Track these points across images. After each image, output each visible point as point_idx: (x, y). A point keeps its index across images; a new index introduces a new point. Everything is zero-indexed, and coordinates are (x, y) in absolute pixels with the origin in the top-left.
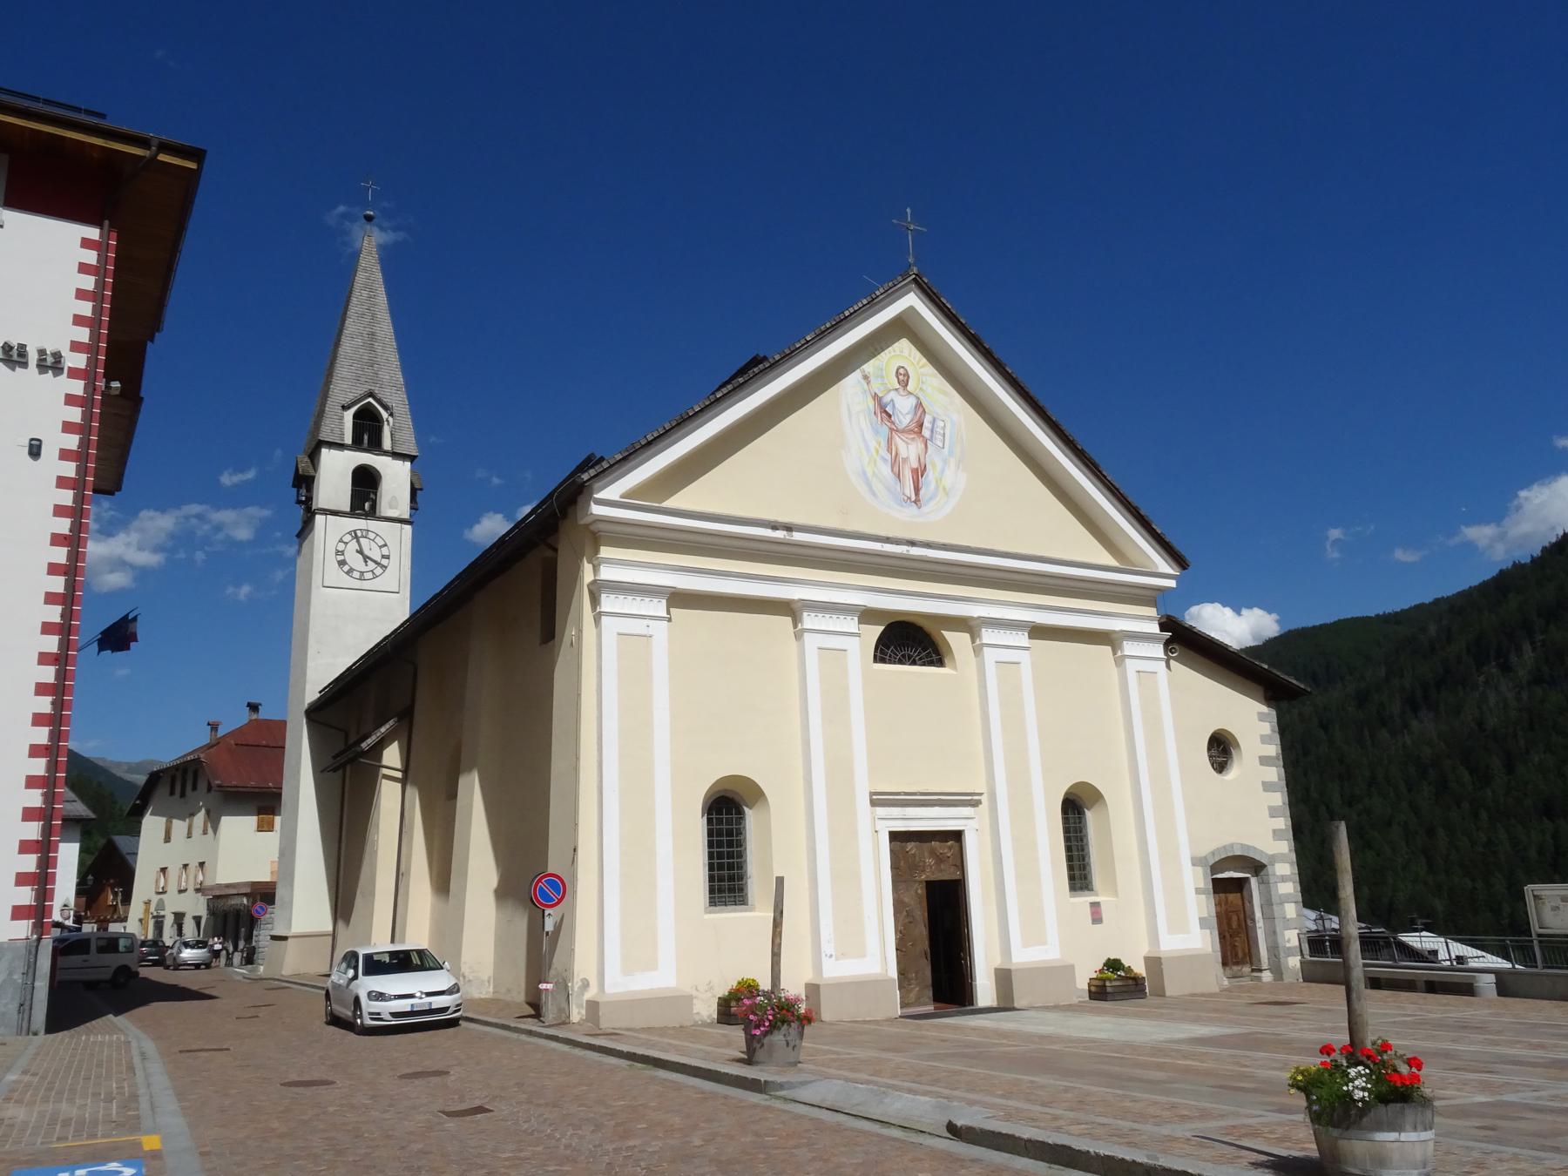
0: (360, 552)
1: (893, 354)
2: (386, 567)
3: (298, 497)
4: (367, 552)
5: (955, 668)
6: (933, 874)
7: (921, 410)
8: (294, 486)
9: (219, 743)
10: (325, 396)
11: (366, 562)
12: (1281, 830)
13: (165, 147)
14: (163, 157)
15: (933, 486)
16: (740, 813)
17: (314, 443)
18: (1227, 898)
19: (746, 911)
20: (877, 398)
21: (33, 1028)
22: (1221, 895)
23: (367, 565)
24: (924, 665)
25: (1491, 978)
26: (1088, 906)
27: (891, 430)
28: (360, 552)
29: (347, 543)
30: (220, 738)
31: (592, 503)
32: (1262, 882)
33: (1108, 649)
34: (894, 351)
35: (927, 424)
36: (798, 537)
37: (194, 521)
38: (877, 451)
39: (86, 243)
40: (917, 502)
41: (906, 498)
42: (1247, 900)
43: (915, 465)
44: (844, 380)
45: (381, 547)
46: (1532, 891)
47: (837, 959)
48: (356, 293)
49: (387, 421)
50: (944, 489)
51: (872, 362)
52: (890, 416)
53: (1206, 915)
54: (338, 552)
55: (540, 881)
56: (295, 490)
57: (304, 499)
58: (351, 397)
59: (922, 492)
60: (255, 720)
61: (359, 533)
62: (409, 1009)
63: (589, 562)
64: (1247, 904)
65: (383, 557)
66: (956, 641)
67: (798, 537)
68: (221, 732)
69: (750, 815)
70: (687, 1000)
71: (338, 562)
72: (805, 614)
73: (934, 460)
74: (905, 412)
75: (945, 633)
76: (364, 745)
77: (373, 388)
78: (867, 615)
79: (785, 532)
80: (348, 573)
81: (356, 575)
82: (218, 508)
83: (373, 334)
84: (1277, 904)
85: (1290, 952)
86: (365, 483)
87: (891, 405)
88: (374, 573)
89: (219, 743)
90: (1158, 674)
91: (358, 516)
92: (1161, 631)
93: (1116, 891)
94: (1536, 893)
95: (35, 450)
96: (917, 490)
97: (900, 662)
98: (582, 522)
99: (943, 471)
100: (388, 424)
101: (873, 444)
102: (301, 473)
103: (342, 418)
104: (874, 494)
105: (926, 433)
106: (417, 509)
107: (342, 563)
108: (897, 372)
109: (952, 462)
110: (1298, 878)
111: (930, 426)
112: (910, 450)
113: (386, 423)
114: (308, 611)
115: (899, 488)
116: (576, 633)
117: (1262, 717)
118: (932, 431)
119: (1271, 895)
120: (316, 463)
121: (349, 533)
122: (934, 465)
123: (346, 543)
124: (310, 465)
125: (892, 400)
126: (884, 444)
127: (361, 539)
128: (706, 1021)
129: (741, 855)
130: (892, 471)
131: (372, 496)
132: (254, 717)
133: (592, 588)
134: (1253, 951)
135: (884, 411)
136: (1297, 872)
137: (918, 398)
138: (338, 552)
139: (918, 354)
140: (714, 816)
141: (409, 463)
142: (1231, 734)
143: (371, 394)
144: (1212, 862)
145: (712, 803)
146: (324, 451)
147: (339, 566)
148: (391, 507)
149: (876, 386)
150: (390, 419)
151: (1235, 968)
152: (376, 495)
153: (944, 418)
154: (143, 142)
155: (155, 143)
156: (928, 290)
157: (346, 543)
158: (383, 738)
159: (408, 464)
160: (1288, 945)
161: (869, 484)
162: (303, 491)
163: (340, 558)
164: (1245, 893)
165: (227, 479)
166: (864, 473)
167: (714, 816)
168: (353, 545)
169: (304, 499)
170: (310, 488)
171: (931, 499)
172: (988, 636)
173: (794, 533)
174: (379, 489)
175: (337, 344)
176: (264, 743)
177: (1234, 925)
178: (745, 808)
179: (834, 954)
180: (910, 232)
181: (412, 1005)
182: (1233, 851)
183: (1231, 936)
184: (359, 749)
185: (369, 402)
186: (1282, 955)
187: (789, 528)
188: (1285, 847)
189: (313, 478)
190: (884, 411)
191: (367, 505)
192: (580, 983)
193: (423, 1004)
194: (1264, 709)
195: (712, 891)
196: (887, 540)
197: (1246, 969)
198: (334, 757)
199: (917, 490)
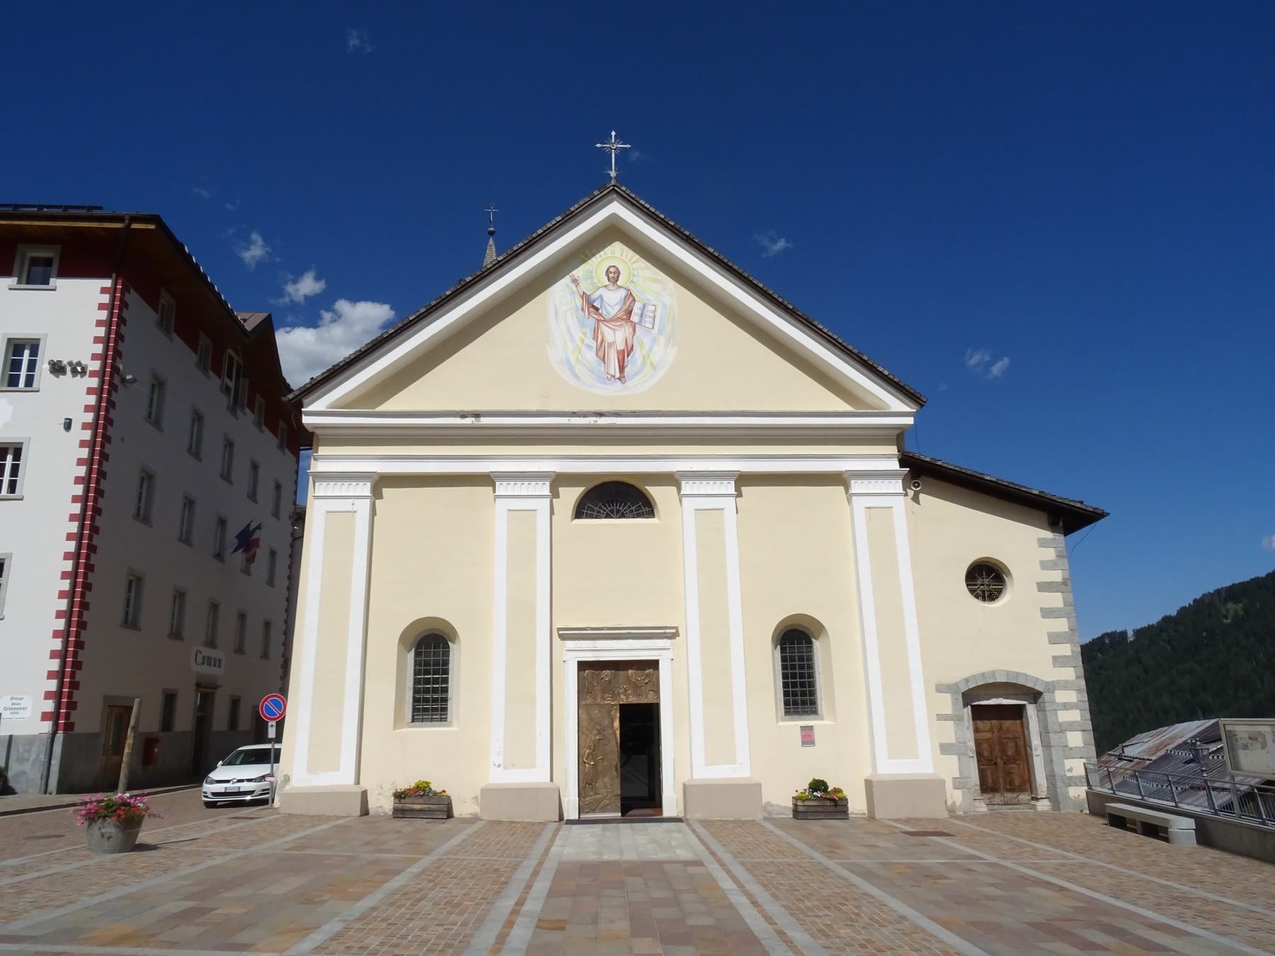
1: (604, 256)
5: (659, 519)
6: (627, 698)
7: (631, 299)
12: (1069, 656)
13: (134, 219)
14: (135, 226)
15: (639, 363)
16: (811, 643)
18: (1001, 726)
19: (445, 726)
20: (585, 297)
21: (49, 789)
22: (993, 722)
24: (634, 517)
25: (1190, 823)
26: (799, 729)
27: (598, 321)
32: (1041, 710)
33: (842, 488)
34: (605, 254)
35: (636, 310)
36: (485, 421)
38: (583, 341)
39: (104, 290)
41: (609, 377)
42: (1024, 727)
43: (621, 346)
44: (552, 287)
46: (1224, 725)
47: (505, 768)
50: (652, 364)
51: (581, 267)
52: (597, 309)
53: (953, 741)
55: (266, 700)
59: (627, 370)
62: (223, 791)
64: (1026, 732)
66: (657, 493)
67: (485, 421)
69: (817, 644)
70: (751, 790)
72: (852, 482)
74: (613, 303)
75: (647, 488)
78: (559, 481)
79: (473, 419)
84: (1056, 732)
85: (1071, 782)
87: (599, 300)
90: (725, 511)
92: (901, 467)
93: (835, 717)
94: (1228, 728)
95: (68, 425)
97: (608, 516)
99: (651, 349)
101: (578, 335)
104: (576, 376)
105: (635, 318)
108: (608, 269)
109: (662, 339)
110: (1088, 706)
111: (639, 312)
112: (616, 336)
115: (602, 369)
117: (1043, 543)
118: (642, 316)
119: (1047, 722)
122: (642, 344)
125: (601, 296)
126: (590, 333)
128: (387, 813)
129: (811, 676)
130: (597, 355)
134: (1032, 778)
135: (591, 306)
136: (1086, 699)
139: (631, 253)
140: (423, 650)
142: (1003, 564)
144: (964, 689)
145: (422, 639)
149: (585, 287)
151: (1009, 795)
153: (656, 303)
154: (119, 219)
155: (127, 217)
156: (627, 197)
160: (1069, 774)
161: (571, 368)
164: (1024, 720)
166: (568, 361)
167: (423, 650)
171: (635, 375)
172: (687, 487)
173: (482, 419)
177: (1010, 752)
178: (813, 639)
179: (502, 764)
180: (613, 151)
181: (226, 788)
182: (995, 678)
183: (1005, 763)
186: (1059, 784)
187: (477, 415)
188: (1072, 673)
190: (591, 306)
192: (282, 778)
193: (234, 787)
194: (1048, 534)
195: (786, 703)
196: (574, 414)
197: (1024, 797)
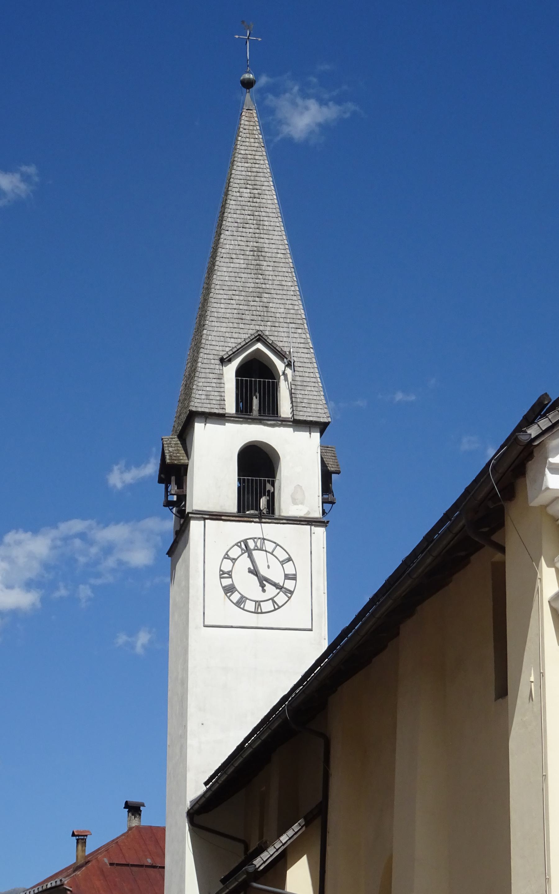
0: (254, 572)
2: (292, 592)
3: (167, 496)
4: (263, 571)
8: (160, 481)
9: (87, 863)
10: (197, 347)
11: (263, 586)
17: (184, 417)
23: (264, 591)
28: (254, 572)
29: (236, 560)
30: (90, 855)
31: (547, 471)
37: (78, 542)
45: (282, 563)
48: (234, 193)
49: (284, 373)
54: (223, 574)
56: (163, 486)
57: (175, 498)
58: (232, 344)
60: (137, 827)
61: (251, 544)
63: (549, 566)
65: (287, 577)
68: (91, 846)
71: (224, 588)
76: (258, 862)
77: (262, 328)
80: (238, 604)
81: (250, 606)
82: (105, 523)
83: (259, 250)
88: (274, 602)
89: (87, 863)
91: (248, 519)
98: (535, 503)
100: (286, 379)
102: (168, 461)
103: (220, 377)
106: (333, 503)
107: (229, 590)
113: (282, 378)
114: (186, 662)
116: (535, 678)
120: (189, 450)
121: (238, 544)
123: (234, 560)
124: (181, 449)
127: (254, 553)
131: (269, 487)
132: (135, 823)
133: (554, 605)
138: (223, 574)
141: (318, 434)
143: (260, 338)
146: (199, 427)
147: (226, 594)
148: (295, 502)
150: (289, 372)
152: (273, 485)
157: (234, 560)
158: (284, 851)
159: (316, 436)
162: (173, 488)
163: (227, 582)
168: (244, 562)
169: (175, 498)
170: (181, 482)
174: (278, 477)
175: (211, 271)
176: (149, 861)
184: (250, 869)
185: (258, 350)
189: (185, 468)
191: (263, 501)
198: (224, 881)
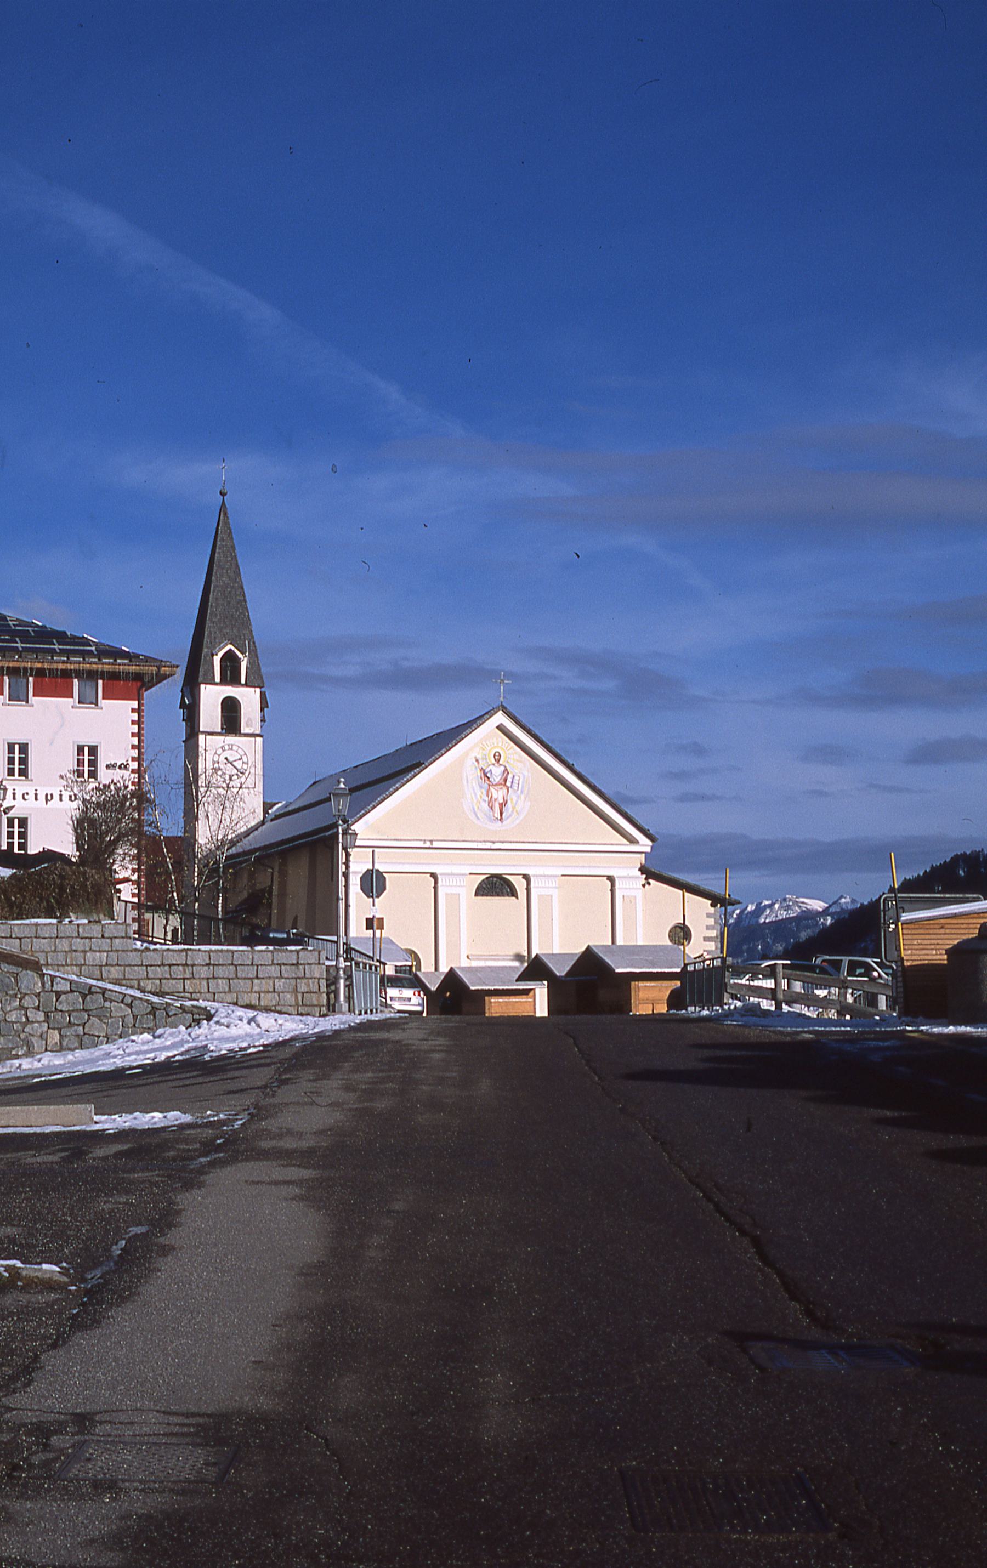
35: (509, 779)
40: (501, 819)
43: (501, 801)
52: (488, 778)
59: (504, 815)
73: (512, 796)
86: (231, 709)
96: (501, 814)
101: (479, 794)
105: (508, 784)
109: (523, 797)
112: (498, 794)
118: (512, 783)
122: (512, 799)
126: (485, 793)
137: (505, 767)
148: (247, 726)
165: (177, 1064)
199: (501, 814)
